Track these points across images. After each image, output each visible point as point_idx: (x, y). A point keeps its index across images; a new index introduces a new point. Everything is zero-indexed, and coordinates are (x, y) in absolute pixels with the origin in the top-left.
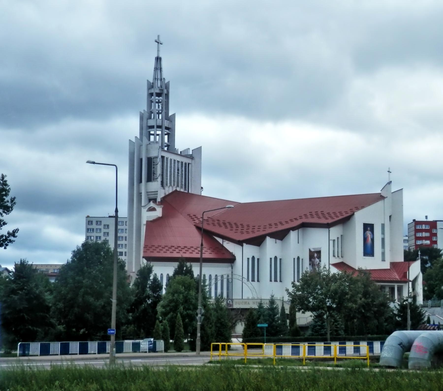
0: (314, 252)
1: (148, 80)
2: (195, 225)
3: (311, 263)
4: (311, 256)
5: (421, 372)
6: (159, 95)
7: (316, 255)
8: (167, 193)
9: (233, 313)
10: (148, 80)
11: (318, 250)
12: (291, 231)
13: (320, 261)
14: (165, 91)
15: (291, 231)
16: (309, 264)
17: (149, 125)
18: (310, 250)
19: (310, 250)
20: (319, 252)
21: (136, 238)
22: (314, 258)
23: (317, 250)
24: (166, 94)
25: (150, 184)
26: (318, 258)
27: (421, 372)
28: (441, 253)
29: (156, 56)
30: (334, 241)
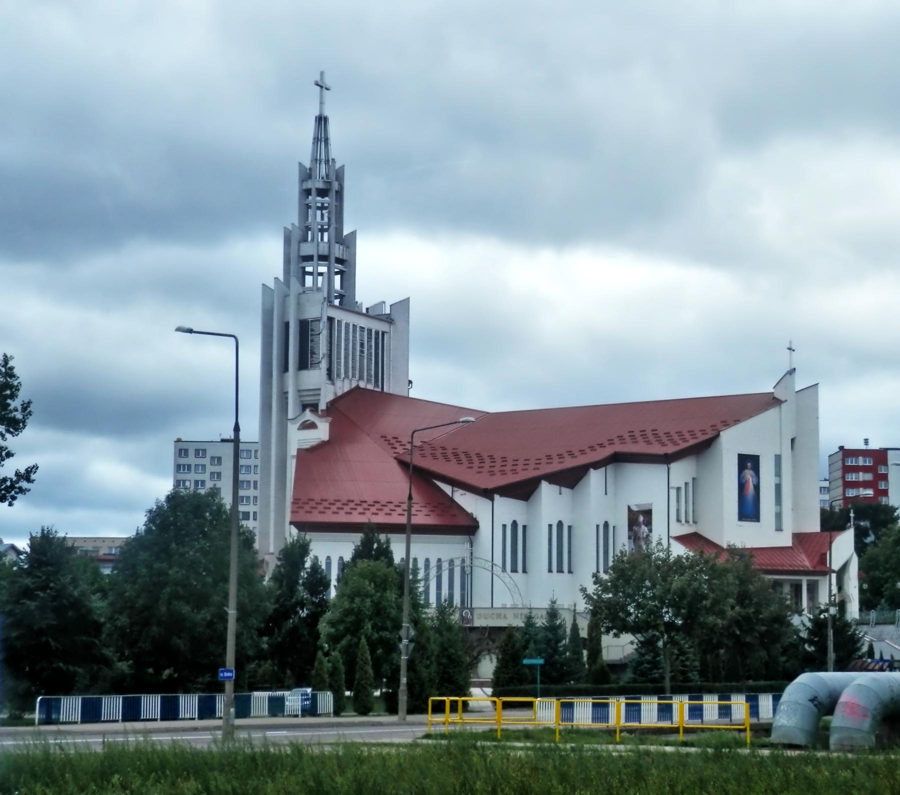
0: (639, 512)
1: (300, 163)
2: (395, 458)
3: (632, 534)
4: (633, 521)
5: (855, 757)
6: (322, 193)
7: (641, 518)
8: (340, 393)
9: (474, 636)
10: (300, 163)
11: (647, 508)
12: (592, 470)
13: (650, 531)
14: (336, 186)
15: (592, 470)
16: (627, 537)
17: (303, 253)
18: (629, 508)
19: (629, 508)
20: (648, 513)
21: (276, 484)
22: (639, 525)
23: (643, 509)
24: (337, 192)
25: (305, 373)
26: (646, 525)
27: (855, 757)
28: (896, 514)
29: (317, 113)
30: (678, 489)
